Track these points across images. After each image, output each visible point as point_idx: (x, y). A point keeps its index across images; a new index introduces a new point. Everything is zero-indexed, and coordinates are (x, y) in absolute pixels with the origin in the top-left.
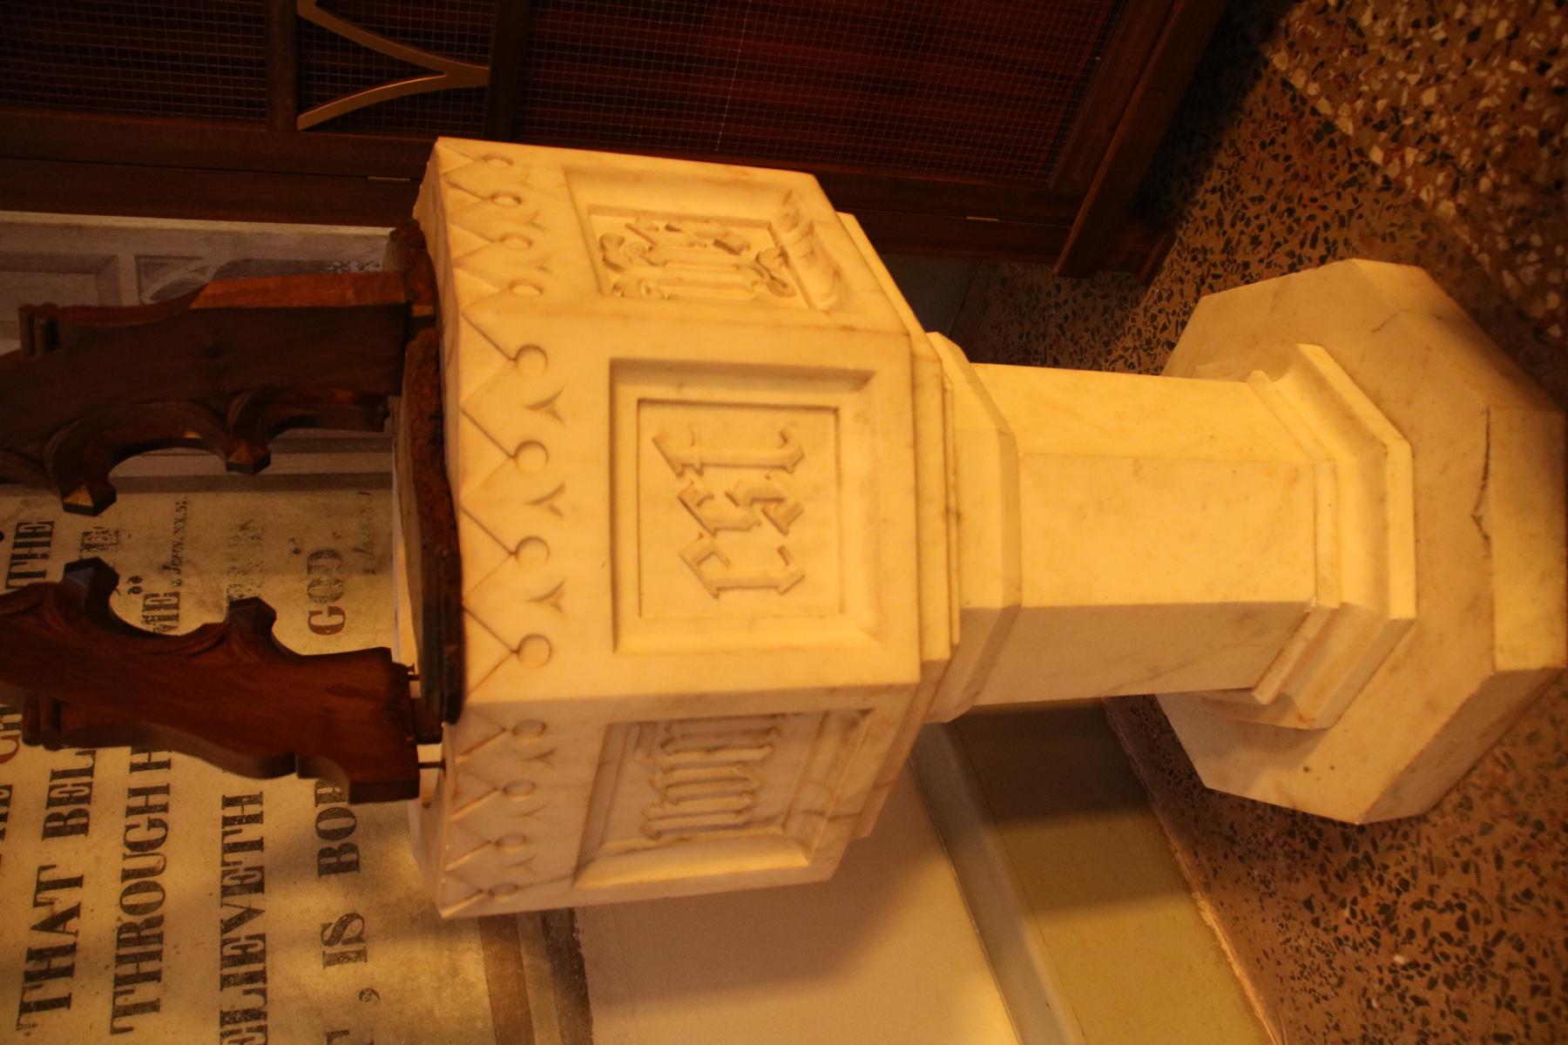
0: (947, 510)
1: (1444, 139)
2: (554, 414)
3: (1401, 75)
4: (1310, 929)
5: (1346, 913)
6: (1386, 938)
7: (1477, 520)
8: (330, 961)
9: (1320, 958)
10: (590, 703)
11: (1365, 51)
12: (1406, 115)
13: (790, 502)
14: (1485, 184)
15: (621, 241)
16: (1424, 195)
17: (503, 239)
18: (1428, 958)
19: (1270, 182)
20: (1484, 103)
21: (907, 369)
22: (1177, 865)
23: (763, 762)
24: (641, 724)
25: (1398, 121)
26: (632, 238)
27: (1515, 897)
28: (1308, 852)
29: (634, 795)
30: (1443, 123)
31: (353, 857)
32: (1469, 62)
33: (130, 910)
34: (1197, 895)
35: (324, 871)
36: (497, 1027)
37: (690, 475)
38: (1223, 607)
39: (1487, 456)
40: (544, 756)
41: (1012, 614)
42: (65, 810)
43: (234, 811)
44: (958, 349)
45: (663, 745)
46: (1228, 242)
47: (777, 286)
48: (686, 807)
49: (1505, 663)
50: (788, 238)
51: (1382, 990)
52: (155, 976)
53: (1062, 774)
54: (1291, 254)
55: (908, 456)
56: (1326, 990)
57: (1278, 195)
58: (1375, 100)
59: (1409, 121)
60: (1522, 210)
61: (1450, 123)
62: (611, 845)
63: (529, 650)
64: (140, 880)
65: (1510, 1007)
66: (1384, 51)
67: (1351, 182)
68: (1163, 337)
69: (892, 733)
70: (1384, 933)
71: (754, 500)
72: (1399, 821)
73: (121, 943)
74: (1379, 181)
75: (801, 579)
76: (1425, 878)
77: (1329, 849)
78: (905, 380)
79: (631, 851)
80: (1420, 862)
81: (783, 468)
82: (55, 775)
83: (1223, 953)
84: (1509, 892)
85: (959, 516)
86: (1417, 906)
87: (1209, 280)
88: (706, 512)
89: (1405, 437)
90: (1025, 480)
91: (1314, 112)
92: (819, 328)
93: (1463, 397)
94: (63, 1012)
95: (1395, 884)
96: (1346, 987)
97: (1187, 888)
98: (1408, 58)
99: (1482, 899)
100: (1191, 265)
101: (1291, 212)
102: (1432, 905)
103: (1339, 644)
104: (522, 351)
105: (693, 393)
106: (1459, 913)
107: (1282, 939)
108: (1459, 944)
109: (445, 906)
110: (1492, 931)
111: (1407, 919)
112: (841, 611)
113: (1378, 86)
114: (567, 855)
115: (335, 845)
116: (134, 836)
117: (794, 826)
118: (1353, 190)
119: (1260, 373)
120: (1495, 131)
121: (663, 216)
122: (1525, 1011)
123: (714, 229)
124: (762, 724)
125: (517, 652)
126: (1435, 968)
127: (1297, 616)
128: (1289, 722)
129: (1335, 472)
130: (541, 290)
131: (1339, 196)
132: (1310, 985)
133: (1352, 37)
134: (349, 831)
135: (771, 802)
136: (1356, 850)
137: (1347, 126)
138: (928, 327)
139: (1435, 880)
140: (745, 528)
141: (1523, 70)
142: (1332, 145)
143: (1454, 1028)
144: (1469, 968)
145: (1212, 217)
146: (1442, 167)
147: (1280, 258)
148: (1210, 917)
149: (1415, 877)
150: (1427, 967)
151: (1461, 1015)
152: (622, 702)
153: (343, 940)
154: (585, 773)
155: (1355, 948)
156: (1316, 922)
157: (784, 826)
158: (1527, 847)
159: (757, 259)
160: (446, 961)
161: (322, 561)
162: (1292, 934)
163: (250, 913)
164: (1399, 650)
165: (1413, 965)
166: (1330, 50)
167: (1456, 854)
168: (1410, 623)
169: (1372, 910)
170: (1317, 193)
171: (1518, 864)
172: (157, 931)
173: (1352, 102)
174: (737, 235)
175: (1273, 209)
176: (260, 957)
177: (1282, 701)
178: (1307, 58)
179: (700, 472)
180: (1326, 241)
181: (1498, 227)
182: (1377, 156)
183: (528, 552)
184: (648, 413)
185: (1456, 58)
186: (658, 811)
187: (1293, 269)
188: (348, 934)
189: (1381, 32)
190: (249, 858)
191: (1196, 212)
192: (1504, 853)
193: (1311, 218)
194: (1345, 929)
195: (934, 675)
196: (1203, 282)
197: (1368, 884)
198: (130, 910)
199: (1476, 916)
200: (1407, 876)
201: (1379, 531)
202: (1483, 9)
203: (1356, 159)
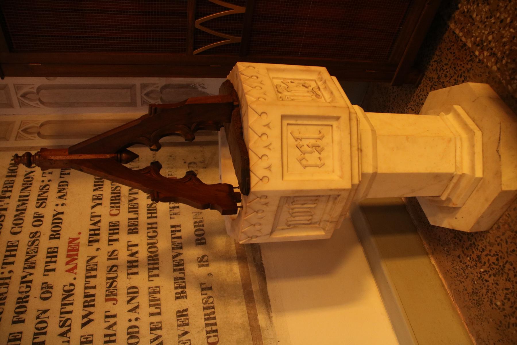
0: (358, 149)
1: (494, 49)
2: (269, 127)
3: (483, 31)
4: (459, 264)
5: (469, 258)
6: (479, 265)
7: (498, 151)
8: (200, 266)
9: (462, 271)
10: (277, 191)
11: (474, 24)
12: (484, 42)
13: (321, 147)
14: (504, 62)
15: (281, 86)
16: (489, 64)
17: (255, 87)
18: (489, 269)
19: (450, 60)
20: (504, 40)
21: (348, 115)
22: (424, 248)
23: (315, 208)
24: (287, 197)
25: (482, 44)
26: (283, 85)
27: (511, 251)
28: (459, 243)
29: (285, 216)
30: (494, 45)
31: (204, 241)
32: (500, 29)
33: (150, 252)
34: (430, 256)
35: (197, 244)
36: (242, 284)
37: (299, 141)
38: (430, 174)
39: (500, 134)
40: (266, 204)
41: (375, 175)
42: (132, 228)
43: (173, 229)
44: (362, 109)
45: (292, 203)
46: (439, 76)
47: (318, 96)
48: (297, 218)
49: (504, 188)
50: (320, 84)
51: (477, 278)
52: (157, 268)
53: (392, 223)
54: (455, 80)
55: (349, 136)
56: (463, 280)
57: (452, 63)
58: (477, 38)
59: (485, 44)
60: (513, 69)
61: (495, 45)
62: (279, 228)
63: (264, 179)
64: (152, 245)
65: (509, 281)
66: (479, 24)
67: (471, 60)
68: (421, 102)
69: (345, 201)
70: (478, 263)
71: (313, 146)
72: (482, 232)
73: (149, 260)
74: (477, 60)
75: (324, 165)
76: (489, 248)
77: (464, 241)
78: (348, 118)
79: (283, 229)
80: (487, 244)
81: (320, 139)
82: (129, 219)
83: (437, 271)
84: (509, 250)
85: (361, 151)
86: (486, 255)
87: (434, 86)
88: (302, 149)
89: (480, 130)
90: (378, 141)
91: (461, 40)
92: (328, 107)
93: (495, 118)
94: (137, 275)
95: (481, 250)
96: (469, 278)
97: (427, 254)
98: (485, 26)
99: (503, 253)
100: (429, 82)
101: (455, 68)
102: (490, 255)
103: (463, 183)
104: (262, 113)
105: (299, 122)
106: (497, 256)
107: (452, 266)
108: (497, 265)
109: (240, 241)
110: (505, 261)
111: (484, 259)
112: (333, 172)
113: (477, 34)
114: (267, 229)
115: (200, 238)
116: (150, 234)
117: (321, 225)
118: (471, 62)
119: (443, 113)
120: (507, 47)
121: (289, 79)
122: (513, 281)
123: (302, 82)
124: (315, 198)
125: (261, 180)
126: (491, 272)
127: (451, 177)
128: (451, 205)
129: (461, 139)
130: (265, 100)
131: (467, 64)
132: (459, 279)
133: (471, 20)
134: (203, 234)
135: (316, 218)
136: (471, 241)
137: (469, 45)
138: (353, 103)
139: (491, 248)
140: (311, 153)
141: (513, 31)
142: (466, 50)
143: (495, 287)
144: (499, 271)
145: (434, 69)
146: (493, 57)
147: (452, 80)
148: (433, 262)
149: (486, 248)
150: (489, 272)
151: (497, 284)
152: (284, 191)
153: (203, 261)
154: (275, 208)
155: (471, 268)
156: (461, 262)
157: (319, 224)
158: (514, 238)
159: (312, 89)
160: (229, 267)
161: (192, 165)
162: (454, 265)
163: (179, 254)
164: (479, 186)
165: (485, 271)
166: (465, 24)
167: (496, 241)
168: (481, 178)
169: (475, 257)
170: (462, 63)
171: (511, 243)
172: (157, 258)
173: (471, 38)
174: (308, 83)
175: (450, 67)
176: (183, 265)
177: (448, 199)
178: (459, 25)
179: (301, 140)
180: (464, 76)
181: (507, 73)
182: (477, 53)
183: (264, 158)
184: (289, 127)
185: (497, 27)
186: (290, 219)
187: (456, 84)
188: (204, 260)
189: (478, 19)
190: (178, 241)
191: (430, 67)
192: (508, 240)
193: (460, 70)
194: (468, 263)
195: (355, 188)
196: (432, 87)
197: (474, 250)
198: (150, 252)
199: (501, 257)
200: (484, 248)
201: (473, 154)
202: (504, 14)
203: (472, 54)
